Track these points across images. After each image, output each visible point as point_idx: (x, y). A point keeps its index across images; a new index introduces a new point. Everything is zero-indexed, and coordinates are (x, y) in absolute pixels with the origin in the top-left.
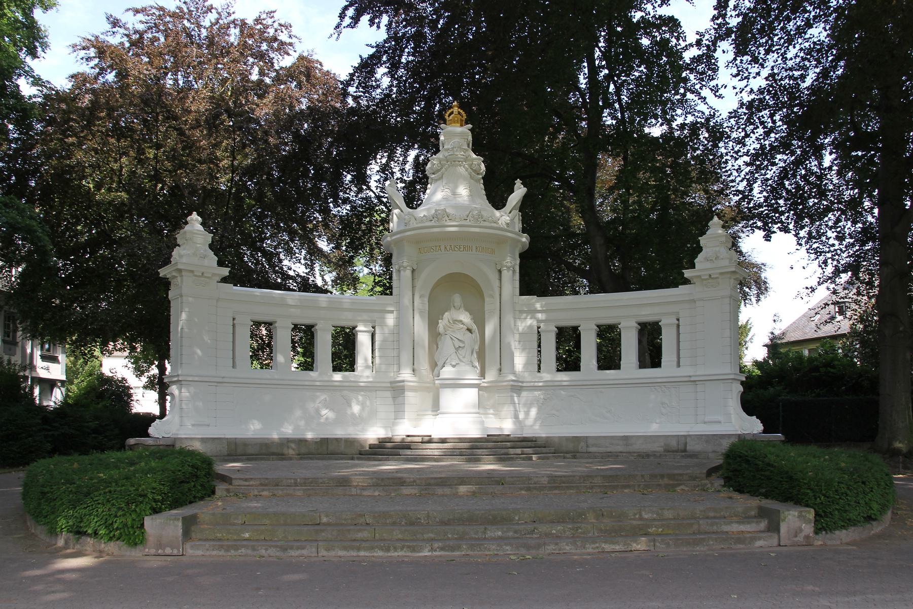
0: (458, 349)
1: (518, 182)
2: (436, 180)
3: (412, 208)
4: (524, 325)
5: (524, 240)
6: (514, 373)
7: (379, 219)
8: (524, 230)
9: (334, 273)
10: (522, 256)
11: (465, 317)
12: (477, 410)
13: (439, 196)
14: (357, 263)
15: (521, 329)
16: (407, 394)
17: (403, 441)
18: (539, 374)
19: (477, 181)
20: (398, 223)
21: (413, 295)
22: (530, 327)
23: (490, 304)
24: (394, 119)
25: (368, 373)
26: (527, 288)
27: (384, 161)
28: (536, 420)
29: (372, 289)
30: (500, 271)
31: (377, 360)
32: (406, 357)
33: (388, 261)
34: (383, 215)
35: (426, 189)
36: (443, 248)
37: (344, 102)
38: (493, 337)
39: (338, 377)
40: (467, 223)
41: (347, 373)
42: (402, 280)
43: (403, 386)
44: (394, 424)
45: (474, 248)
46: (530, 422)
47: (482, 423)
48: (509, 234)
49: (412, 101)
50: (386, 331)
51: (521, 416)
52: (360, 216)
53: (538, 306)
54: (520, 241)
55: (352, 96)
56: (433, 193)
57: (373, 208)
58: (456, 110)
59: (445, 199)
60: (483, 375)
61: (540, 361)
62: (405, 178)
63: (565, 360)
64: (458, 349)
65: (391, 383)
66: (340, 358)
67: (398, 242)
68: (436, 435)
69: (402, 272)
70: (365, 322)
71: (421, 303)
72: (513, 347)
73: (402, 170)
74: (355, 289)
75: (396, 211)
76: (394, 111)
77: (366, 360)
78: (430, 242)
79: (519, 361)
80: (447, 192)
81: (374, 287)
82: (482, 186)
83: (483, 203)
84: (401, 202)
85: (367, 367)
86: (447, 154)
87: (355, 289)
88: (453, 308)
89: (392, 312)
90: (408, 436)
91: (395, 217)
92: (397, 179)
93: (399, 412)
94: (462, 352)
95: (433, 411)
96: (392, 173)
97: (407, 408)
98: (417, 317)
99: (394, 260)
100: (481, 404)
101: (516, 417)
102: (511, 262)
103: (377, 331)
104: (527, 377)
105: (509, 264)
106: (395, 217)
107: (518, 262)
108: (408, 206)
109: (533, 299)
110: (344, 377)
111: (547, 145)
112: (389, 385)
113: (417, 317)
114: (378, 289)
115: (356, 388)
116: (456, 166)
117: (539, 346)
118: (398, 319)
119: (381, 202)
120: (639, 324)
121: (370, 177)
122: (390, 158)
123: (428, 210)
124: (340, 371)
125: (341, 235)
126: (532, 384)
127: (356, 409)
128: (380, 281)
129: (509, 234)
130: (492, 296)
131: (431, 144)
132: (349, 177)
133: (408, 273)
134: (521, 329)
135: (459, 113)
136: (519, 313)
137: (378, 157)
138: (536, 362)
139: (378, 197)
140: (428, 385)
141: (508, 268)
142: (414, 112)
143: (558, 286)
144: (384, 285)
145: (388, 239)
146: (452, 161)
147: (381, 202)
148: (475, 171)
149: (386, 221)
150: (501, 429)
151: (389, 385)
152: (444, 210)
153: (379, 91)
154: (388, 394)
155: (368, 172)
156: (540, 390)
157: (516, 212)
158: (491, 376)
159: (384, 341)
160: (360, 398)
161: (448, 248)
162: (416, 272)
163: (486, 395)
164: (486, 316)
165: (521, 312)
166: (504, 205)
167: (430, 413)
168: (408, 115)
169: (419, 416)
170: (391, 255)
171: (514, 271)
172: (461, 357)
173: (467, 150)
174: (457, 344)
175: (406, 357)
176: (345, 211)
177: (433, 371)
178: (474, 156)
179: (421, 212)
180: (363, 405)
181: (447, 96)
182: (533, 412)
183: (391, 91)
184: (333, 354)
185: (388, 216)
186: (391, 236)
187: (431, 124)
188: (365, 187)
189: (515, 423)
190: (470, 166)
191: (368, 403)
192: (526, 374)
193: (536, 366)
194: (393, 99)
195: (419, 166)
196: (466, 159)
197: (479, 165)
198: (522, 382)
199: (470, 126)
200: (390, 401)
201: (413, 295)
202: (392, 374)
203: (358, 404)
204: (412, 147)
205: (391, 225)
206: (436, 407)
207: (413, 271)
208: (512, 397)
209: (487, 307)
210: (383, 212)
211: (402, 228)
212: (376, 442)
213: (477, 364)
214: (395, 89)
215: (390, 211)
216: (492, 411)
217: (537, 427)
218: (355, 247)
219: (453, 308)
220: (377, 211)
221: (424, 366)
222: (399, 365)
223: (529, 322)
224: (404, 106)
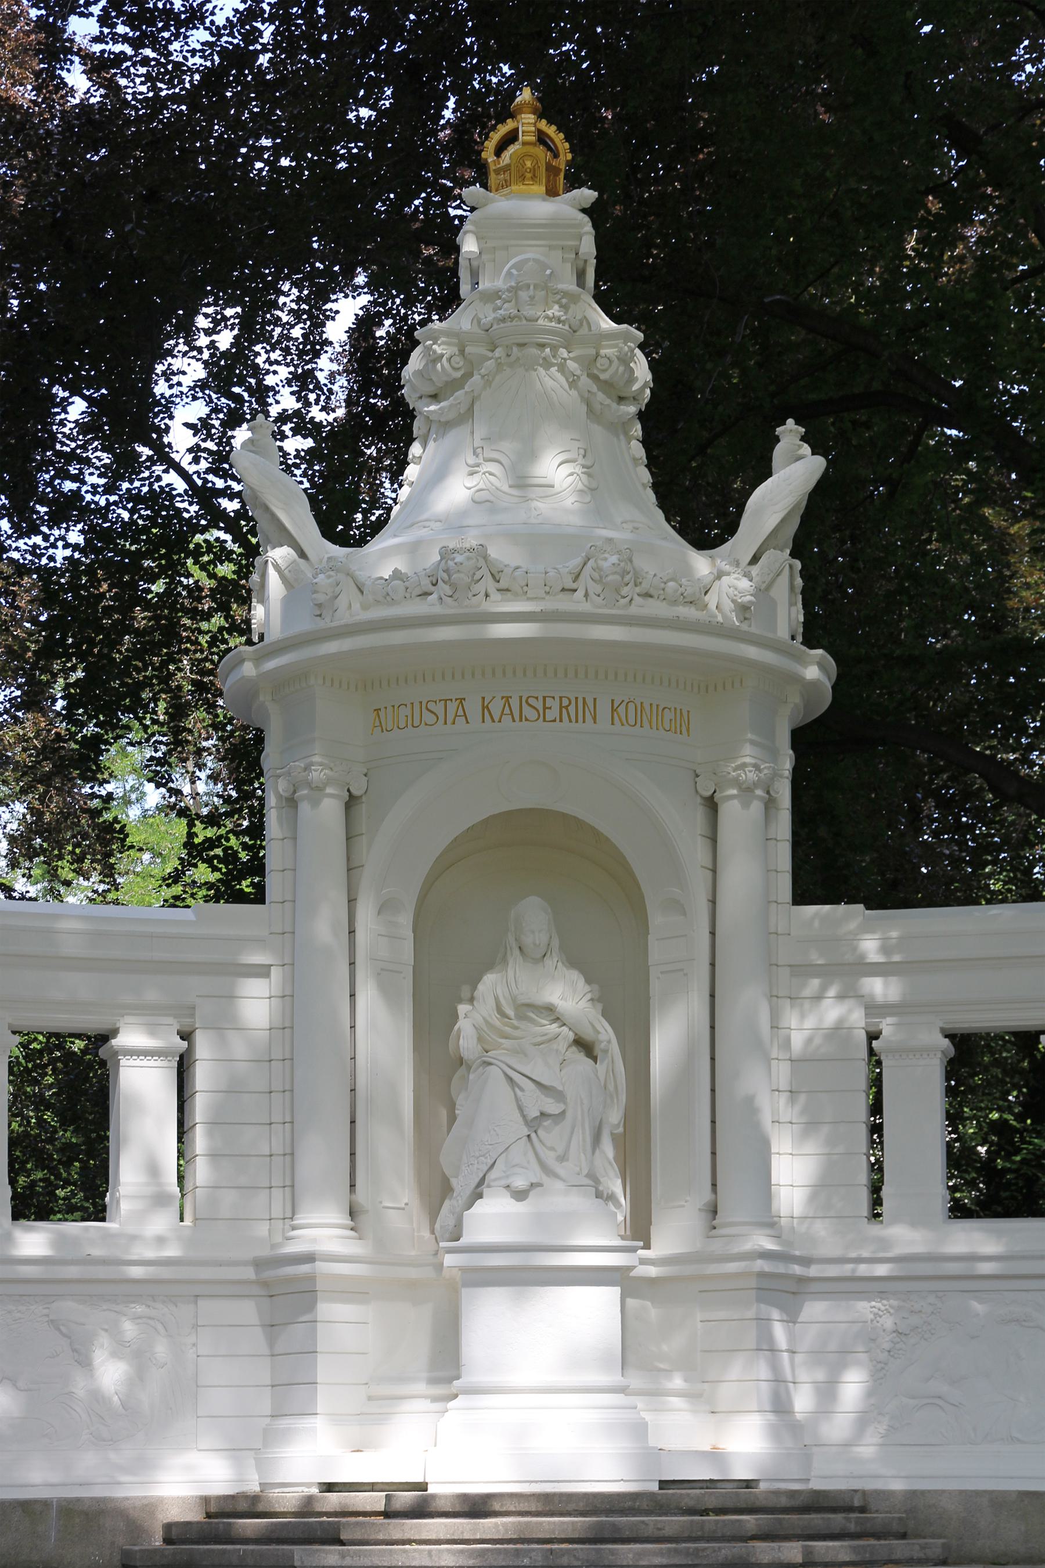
0: (535, 1123)
1: (790, 432)
2: (446, 426)
3: (343, 540)
4: (810, 1023)
5: (812, 673)
6: (770, 1223)
7: (208, 583)
8: (812, 635)
9: (20, 808)
10: (800, 738)
11: (567, 994)
12: (615, 1378)
13: (457, 491)
14: (117, 767)
15: (798, 1040)
16: (328, 1310)
17: (307, 1508)
18: (875, 1230)
19: (620, 428)
20: (288, 602)
21: (352, 901)
22: (838, 1032)
23: (673, 941)
24: (267, 158)
25: (161, 1223)
26: (819, 878)
27: (225, 340)
28: (863, 1420)
29: (175, 877)
30: (712, 805)
31: (201, 1172)
32: (320, 1155)
33: (244, 757)
34: (225, 570)
35: (402, 464)
36: (473, 707)
37: (50, 84)
38: (684, 1075)
39: (34, 1241)
40: (576, 603)
41: (74, 1228)
42: (303, 840)
43: (311, 1278)
44: (271, 1437)
45: (604, 710)
46: (838, 1427)
47: (640, 1430)
48: (752, 652)
49: (343, 87)
50: (239, 1049)
51: (803, 1402)
52: (127, 574)
53: (870, 947)
54: (797, 679)
55: (86, 57)
56: (438, 477)
57: (183, 539)
58: (527, 123)
59: (481, 502)
60: (640, 1230)
61: (877, 1168)
62: (316, 413)
63: (987, 1168)
64: (535, 1123)
65: (259, 1264)
66: (43, 1161)
67: (284, 684)
68: (446, 1482)
69: (304, 807)
70: (149, 1013)
71: (383, 934)
72: (766, 1118)
73: (303, 381)
74: (109, 872)
75: (279, 555)
76: (264, 125)
77: (153, 1170)
78: (423, 686)
79: (793, 1172)
80: (492, 476)
81: (187, 864)
82: (638, 451)
83: (640, 521)
84: (296, 514)
85: (160, 1200)
86: (488, 315)
87: (109, 872)
88: (515, 958)
89: (262, 971)
90: (329, 1487)
91: (274, 583)
92: (283, 418)
93: (289, 1389)
94: (551, 1136)
95: (433, 1381)
96: (262, 393)
97: (325, 1370)
98: (368, 996)
99: (270, 758)
100: (633, 1352)
101: (780, 1405)
102: (759, 771)
103: (203, 1049)
104: (825, 1239)
105: (751, 776)
106: (272, 575)
107: (787, 762)
108: (328, 533)
109: (849, 916)
110: (59, 1242)
111: (914, 271)
112: (249, 1273)
113: (368, 996)
114: (203, 873)
115: (111, 1288)
116: (530, 367)
117: (876, 1108)
118: (292, 1002)
119: (217, 517)
120: (950, 1036)
121: (167, 407)
122: (251, 331)
123: (414, 549)
124: (43, 1214)
125: (49, 651)
126: (847, 1269)
127: (110, 1373)
128: (211, 843)
129: (752, 652)
130: (678, 907)
131: (422, 269)
132: (77, 408)
133: (329, 810)
134: (798, 1040)
135: (542, 139)
136: (792, 977)
137: (202, 322)
138: (862, 1177)
139: (204, 495)
140: (413, 1273)
141: (747, 791)
142: (353, 132)
143: (956, 862)
144: (230, 857)
145: (243, 669)
146: (512, 346)
147: (217, 517)
148: (606, 386)
149: (235, 594)
150: (715, 1456)
151: (249, 1273)
152: (481, 552)
153: (199, 36)
154: (247, 1311)
155: (161, 388)
156: (882, 1295)
157: (780, 558)
158: (673, 1235)
159: (231, 1090)
160: (129, 1328)
161: (496, 708)
162: (363, 810)
163: (653, 1313)
164: (655, 986)
165: (802, 971)
166: (731, 528)
167: (421, 1388)
168: (325, 143)
169: (376, 1408)
170: (259, 739)
171: (770, 804)
172: (549, 1157)
173: (574, 299)
174: (536, 1103)
175: (320, 1155)
176: (61, 554)
177: (433, 1213)
178: (606, 324)
179: (384, 558)
180: (140, 1359)
181: (490, 59)
182: (853, 1386)
183: (253, 36)
184: (14, 1142)
185: (244, 571)
186: (258, 660)
187: (423, 184)
188: (145, 451)
189: (775, 1433)
190: (589, 364)
191: (161, 1349)
192: (821, 1229)
193: (864, 1196)
194: (261, 72)
195: (375, 362)
196: (574, 334)
197: (626, 360)
198: (806, 1261)
199: (587, 195)
200: (257, 1339)
201: (352, 901)
202: (262, 1229)
203: (115, 1355)
204: (344, 284)
205: (258, 612)
206: (445, 1365)
207: (351, 802)
208: (763, 1323)
209: (656, 952)
210: (222, 555)
211: (305, 624)
212: (195, 1516)
213: (616, 1186)
214: (268, 31)
215: (252, 551)
216: (677, 1382)
217: (867, 1450)
218: (108, 699)
219: (515, 958)
220: (196, 554)
221: (397, 1197)
222: (292, 1187)
223: (832, 1012)
224: (307, 105)
